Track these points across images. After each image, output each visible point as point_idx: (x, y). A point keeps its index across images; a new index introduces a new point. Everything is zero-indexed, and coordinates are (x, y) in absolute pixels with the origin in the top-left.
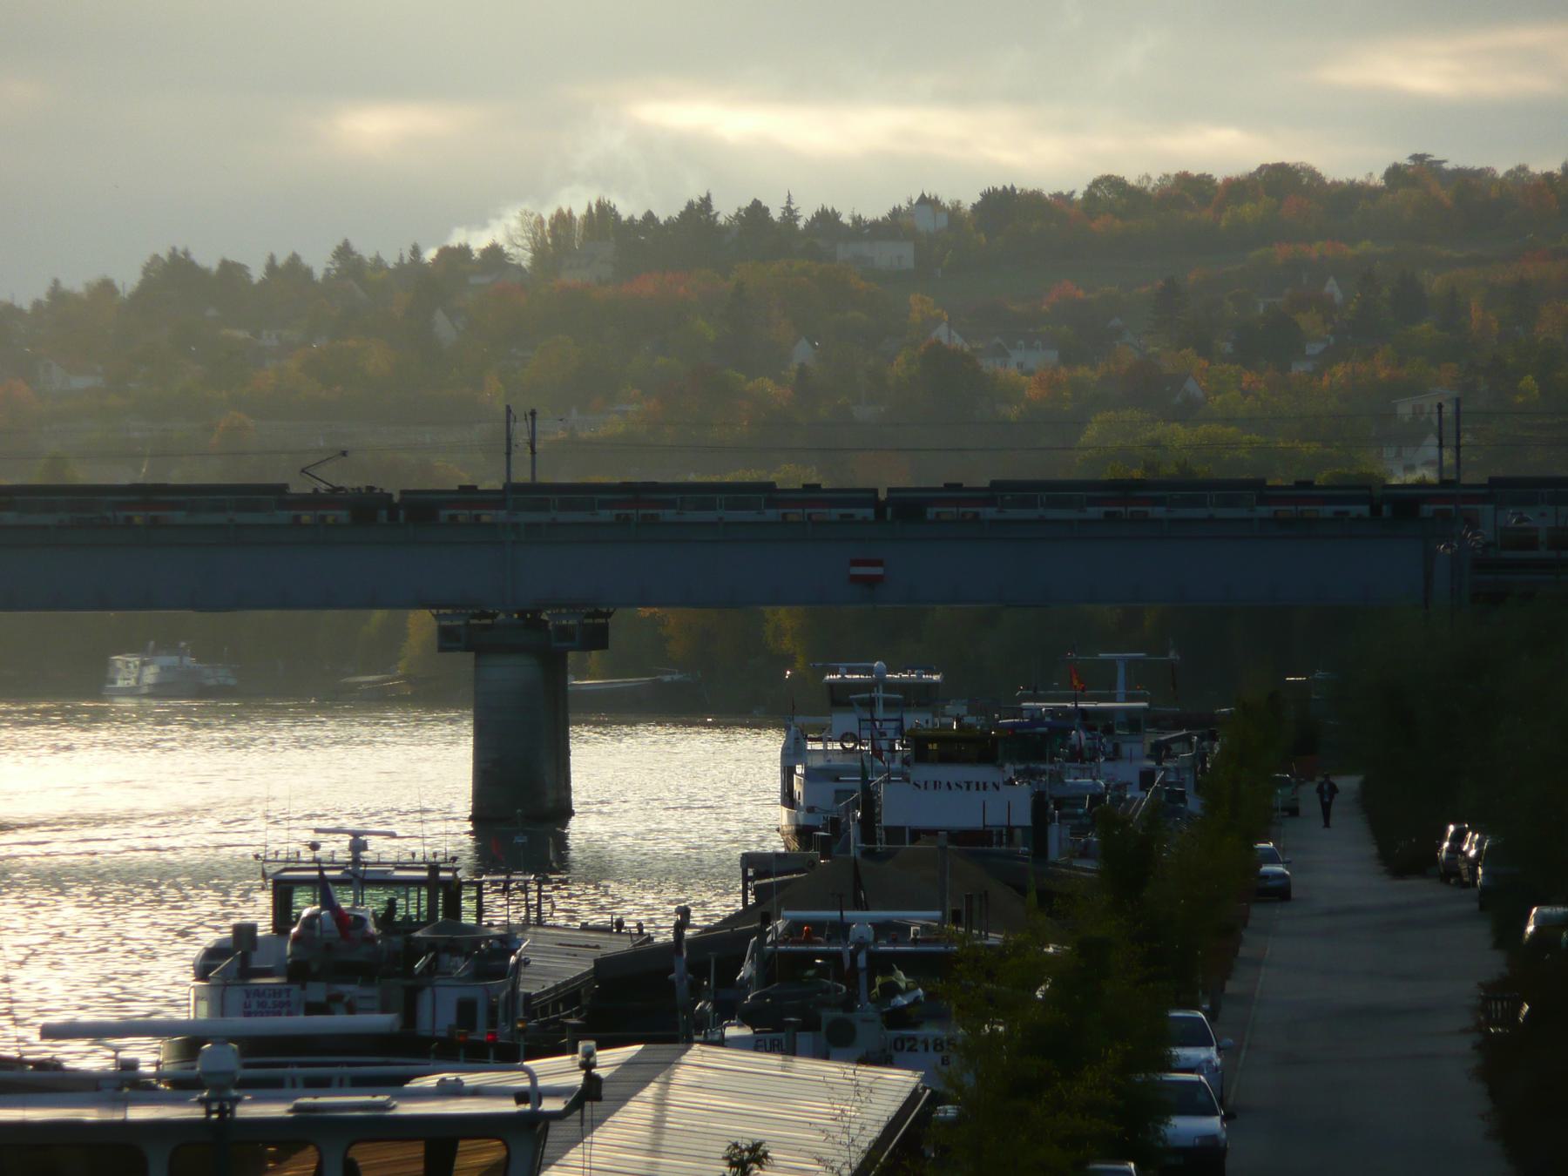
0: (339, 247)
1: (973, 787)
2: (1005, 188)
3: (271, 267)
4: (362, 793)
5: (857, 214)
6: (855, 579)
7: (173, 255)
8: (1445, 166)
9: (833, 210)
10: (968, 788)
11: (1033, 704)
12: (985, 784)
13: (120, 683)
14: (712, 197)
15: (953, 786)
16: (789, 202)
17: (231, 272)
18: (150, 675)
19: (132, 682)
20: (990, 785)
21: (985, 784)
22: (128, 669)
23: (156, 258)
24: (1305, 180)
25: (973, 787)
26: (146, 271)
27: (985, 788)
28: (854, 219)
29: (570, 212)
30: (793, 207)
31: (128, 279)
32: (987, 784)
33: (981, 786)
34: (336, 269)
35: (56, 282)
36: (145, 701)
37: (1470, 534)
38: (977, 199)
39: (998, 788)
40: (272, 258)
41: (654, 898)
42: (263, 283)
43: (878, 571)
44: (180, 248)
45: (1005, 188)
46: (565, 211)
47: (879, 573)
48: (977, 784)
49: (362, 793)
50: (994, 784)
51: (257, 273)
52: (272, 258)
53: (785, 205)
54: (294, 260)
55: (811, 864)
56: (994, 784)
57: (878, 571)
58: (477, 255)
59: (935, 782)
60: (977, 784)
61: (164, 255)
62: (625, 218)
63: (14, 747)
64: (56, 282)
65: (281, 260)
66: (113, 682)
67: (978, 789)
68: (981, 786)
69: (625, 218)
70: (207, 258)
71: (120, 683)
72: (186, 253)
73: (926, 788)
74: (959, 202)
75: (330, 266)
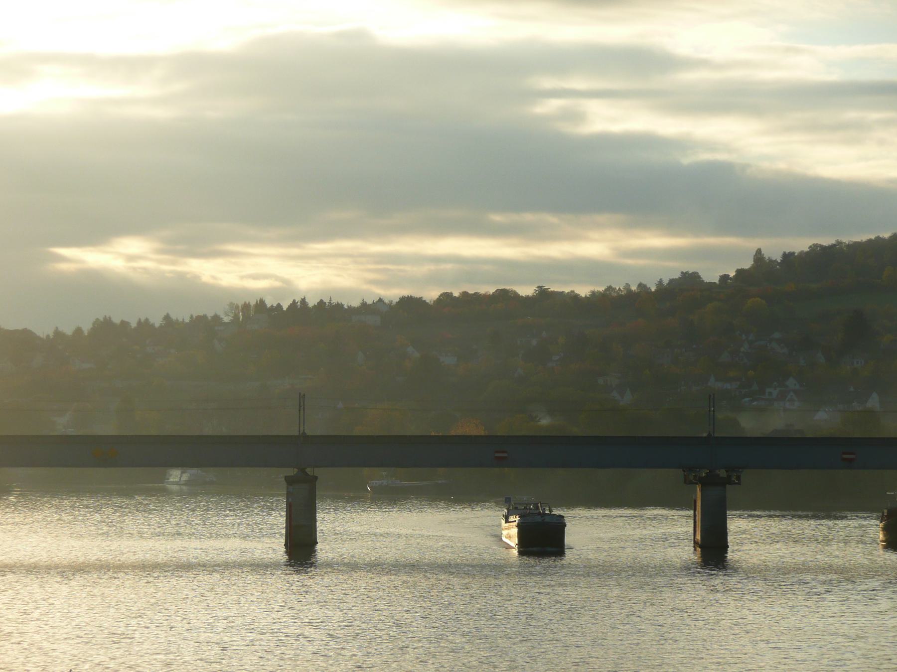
0: (165, 316)
2: (408, 296)
3: (139, 323)
4: (621, 640)
5: (349, 305)
6: (497, 457)
7: (105, 318)
9: (341, 303)
13: (171, 480)
14: (306, 299)
16: (330, 300)
17: (124, 324)
18: (185, 477)
19: (177, 479)
22: (176, 475)
23: (97, 319)
24: (535, 294)
26: (94, 324)
28: (348, 306)
29: (249, 303)
30: (332, 302)
31: (86, 327)
34: (164, 324)
35: (57, 328)
36: (182, 487)
38: (398, 300)
40: (140, 319)
42: (719, 283)
43: (505, 455)
44: (108, 316)
45: (408, 296)
46: (247, 303)
49: (621, 640)
51: (134, 325)
52: (140, 319)
53: (329, 301)
54: (147, 320)
57: (505, 455)
58: (210, 318)
61: (102, 319)
62: (269, 306)
64: (57, 328)
65: (142, 320)
66: (168, 479)
69: (269, 306)
70: (117, 320)
71: (171, 480)
72: (110, 318)
74: (392, 301)
75: (162, 323)
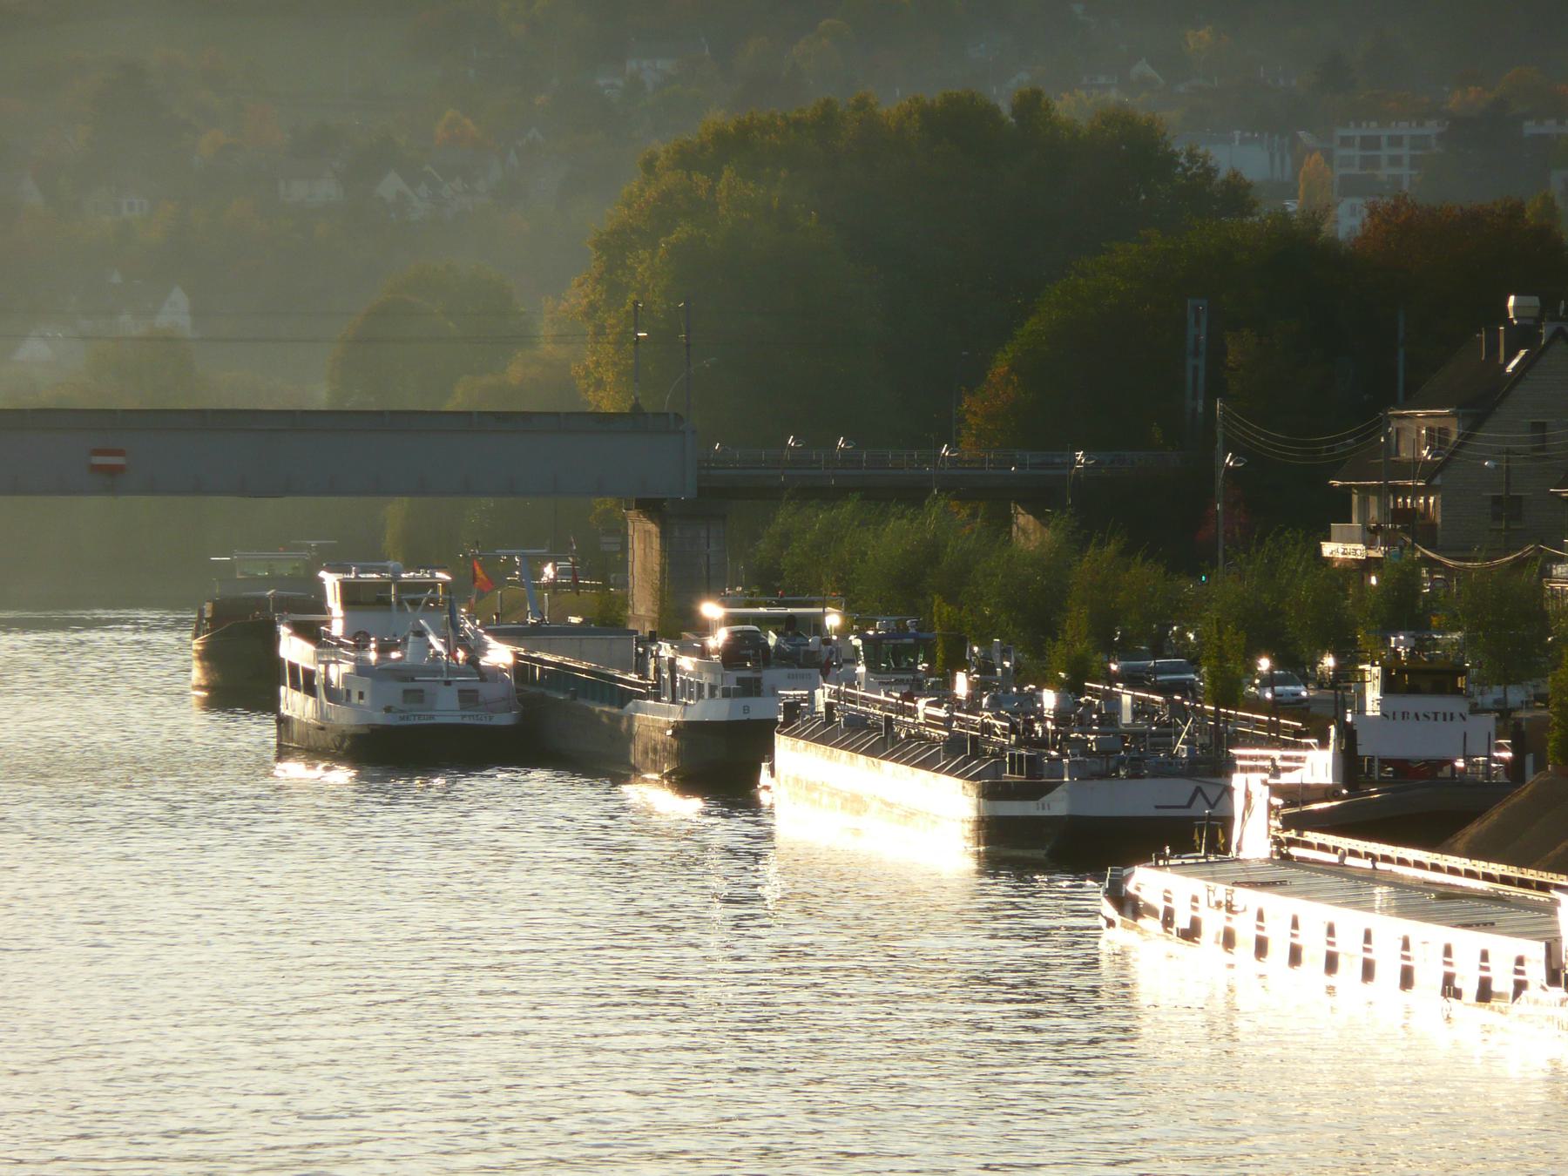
1: (1440, 717)
8: (764, 767)
10: (1436, 719)
11: (1147, 695)
12: (1452, 714)
15: (1421, 717)
20: (1456, 715)
21: (1452, 714)
25: (1440, 717)
27: (1452, 719)
32: (1454, 715)
33: (1448, 717)
37: (1409, 501)
39: (1464, 719)
41: (355, 791)
43: (98, 460)
47: (97, 457)
48: (1445, 714)
50: (1461, 715)
55: (1336, 794)
56: (1461, 715)
57: (98, 460)
59: (1403, 713)
60: (1445, 714)
63: (909, 815)
67: (1445, 720)
68: (1448, 717)
73: (1394, 718)
